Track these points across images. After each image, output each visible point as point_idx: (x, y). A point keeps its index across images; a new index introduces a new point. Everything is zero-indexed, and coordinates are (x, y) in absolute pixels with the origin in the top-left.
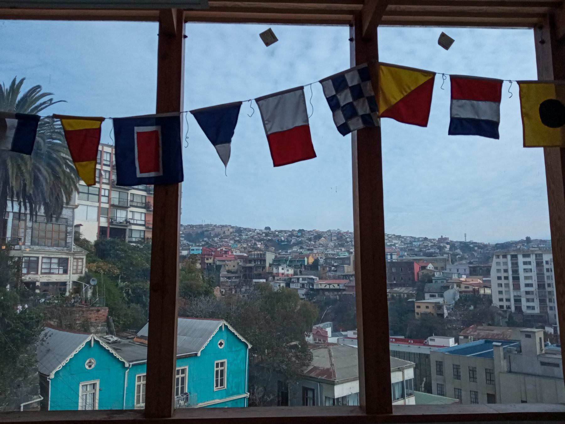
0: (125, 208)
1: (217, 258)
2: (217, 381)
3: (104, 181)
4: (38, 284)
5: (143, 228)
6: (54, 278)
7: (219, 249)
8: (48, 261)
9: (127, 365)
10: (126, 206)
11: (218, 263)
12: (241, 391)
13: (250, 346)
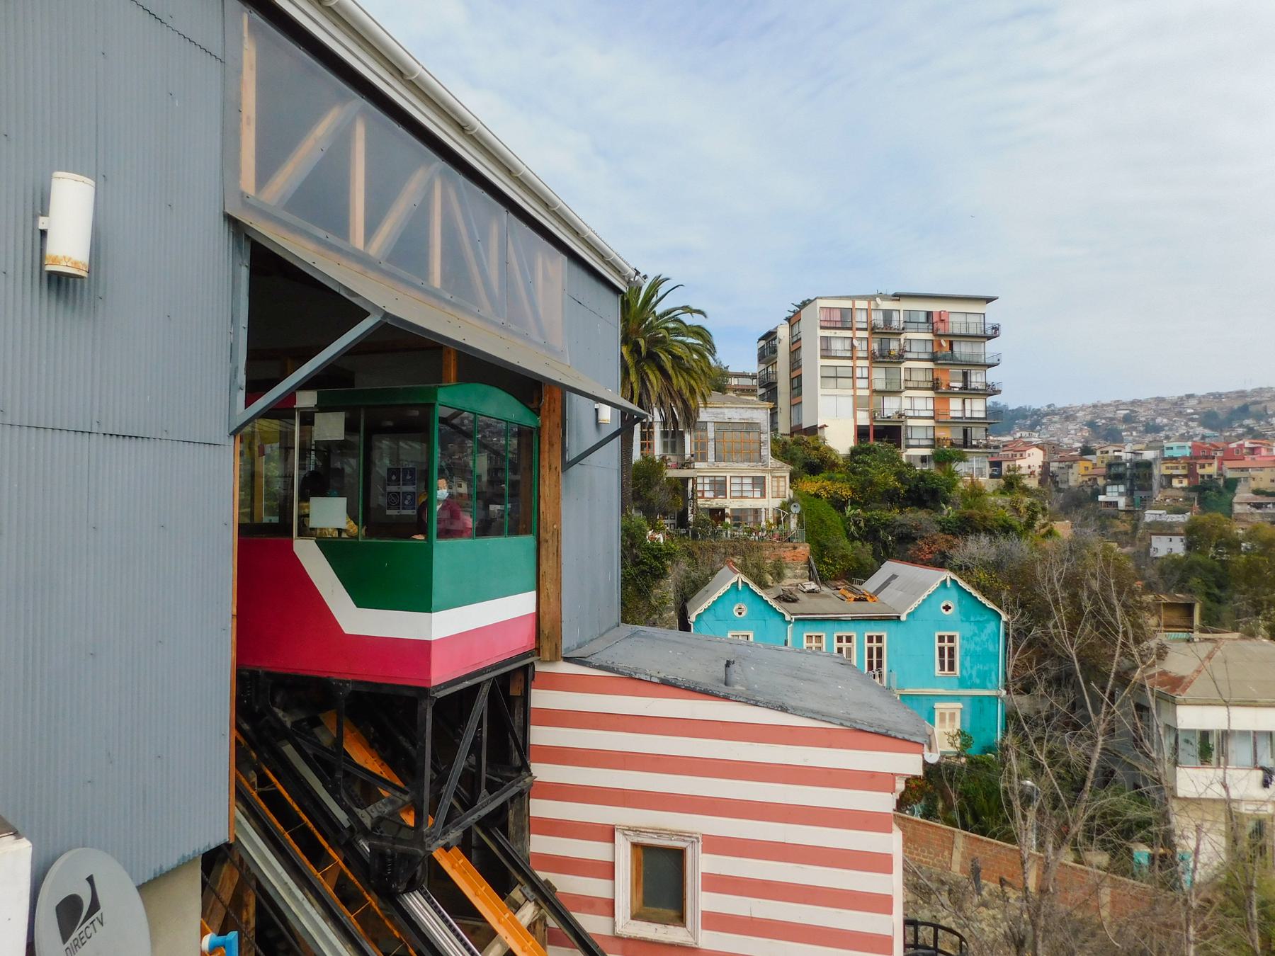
0: (897, 393)
1: (1227, 464)
2: (942, 663)
3: (861, 354)
4: (727, 511)
5: (931, 423)
6: (747, 504)
7: (1234, 445)
8: (738, 480)
9: (788, 618)
10: (895, 388)
11: (1230, 474)
12: (989, 685)
13: (1004, 618)
